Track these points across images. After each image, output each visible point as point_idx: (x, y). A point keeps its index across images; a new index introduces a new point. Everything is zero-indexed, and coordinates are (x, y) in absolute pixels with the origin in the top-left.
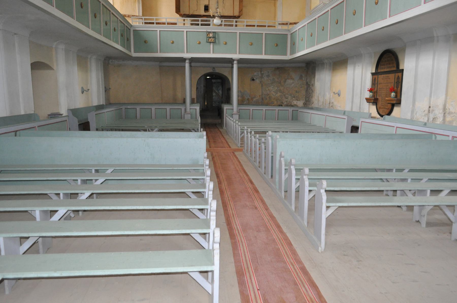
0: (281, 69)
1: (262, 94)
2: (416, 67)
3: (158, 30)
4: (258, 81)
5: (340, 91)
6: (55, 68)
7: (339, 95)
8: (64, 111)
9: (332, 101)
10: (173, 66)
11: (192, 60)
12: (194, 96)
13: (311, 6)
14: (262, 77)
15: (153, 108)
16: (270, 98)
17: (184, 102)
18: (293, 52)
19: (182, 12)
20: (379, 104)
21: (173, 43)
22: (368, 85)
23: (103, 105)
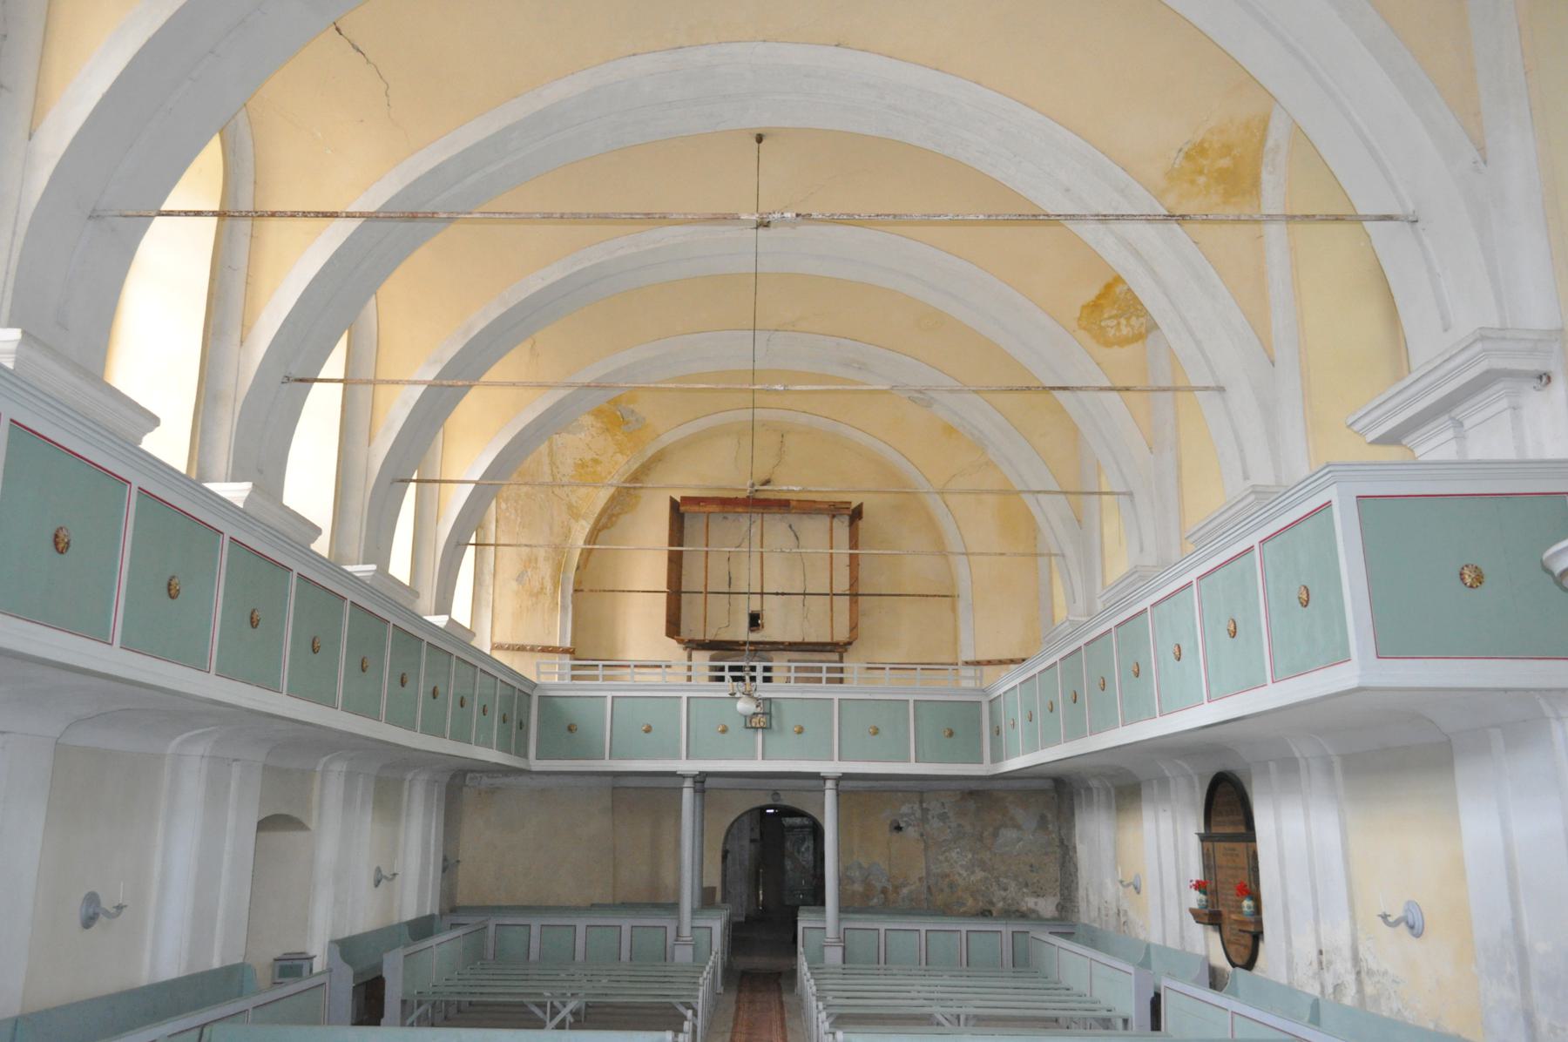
0: (983, 797)
1: (928, 874)
2: (1286, 830)
3: (609, 695)
4: (911, 832)
5: (1137, 876)
6: (313, 825)
7: (1138, 890)
8: (318, 949)
9: (1125, 905)
10: (646, 796)
11: (701, 779)
12: (714, 879)
13: (1053, 616)
14: (924, 820)
15: (581, 923)
16: (952, 886)
17: (674, 907)
18: (996, 758)
19: (685, 635)
20: (1226, 928)
21: (648, 730)
22: (1196, 872)
23: (432, 916)
